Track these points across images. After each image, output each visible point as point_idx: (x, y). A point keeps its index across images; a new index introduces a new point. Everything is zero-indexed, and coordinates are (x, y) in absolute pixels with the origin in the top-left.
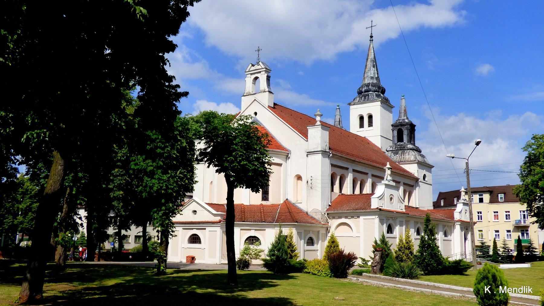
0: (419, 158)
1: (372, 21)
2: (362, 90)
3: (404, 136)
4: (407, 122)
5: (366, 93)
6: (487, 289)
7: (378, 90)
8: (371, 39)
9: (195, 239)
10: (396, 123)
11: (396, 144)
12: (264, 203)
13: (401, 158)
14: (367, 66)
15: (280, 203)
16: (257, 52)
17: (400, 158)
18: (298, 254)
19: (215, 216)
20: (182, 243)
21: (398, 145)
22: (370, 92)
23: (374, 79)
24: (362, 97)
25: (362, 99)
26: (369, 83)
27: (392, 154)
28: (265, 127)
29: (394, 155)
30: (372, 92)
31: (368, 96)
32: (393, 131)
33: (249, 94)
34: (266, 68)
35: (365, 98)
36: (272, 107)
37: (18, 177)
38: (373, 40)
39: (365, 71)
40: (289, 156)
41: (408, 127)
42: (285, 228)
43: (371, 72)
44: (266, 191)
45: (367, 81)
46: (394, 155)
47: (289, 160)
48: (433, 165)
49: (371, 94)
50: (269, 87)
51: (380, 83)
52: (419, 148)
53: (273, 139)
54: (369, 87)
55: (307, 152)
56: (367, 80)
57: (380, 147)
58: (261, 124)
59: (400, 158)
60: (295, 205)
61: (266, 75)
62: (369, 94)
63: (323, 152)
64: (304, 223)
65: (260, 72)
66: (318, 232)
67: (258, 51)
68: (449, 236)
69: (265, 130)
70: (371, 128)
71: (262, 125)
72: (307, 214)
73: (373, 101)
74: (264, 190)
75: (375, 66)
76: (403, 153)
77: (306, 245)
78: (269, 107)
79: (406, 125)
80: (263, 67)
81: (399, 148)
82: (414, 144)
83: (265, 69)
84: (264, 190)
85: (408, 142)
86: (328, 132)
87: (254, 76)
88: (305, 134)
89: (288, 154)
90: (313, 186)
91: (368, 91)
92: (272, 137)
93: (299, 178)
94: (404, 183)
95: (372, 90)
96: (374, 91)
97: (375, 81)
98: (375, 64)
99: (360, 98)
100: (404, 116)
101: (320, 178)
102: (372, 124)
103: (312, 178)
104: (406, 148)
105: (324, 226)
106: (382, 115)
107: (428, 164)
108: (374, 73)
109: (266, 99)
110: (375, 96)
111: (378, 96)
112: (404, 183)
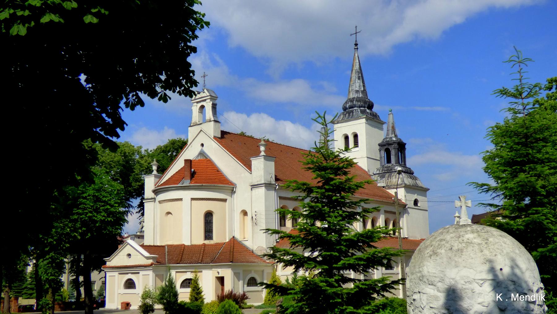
0: (408, 181)
1: (356, 27)
2: (346, 106)
3: (391, 156)
4: (395, 141)
5: (351, 109)
6: (499, 297)
7: (364, 105)
8: (356, 47)
9: (131, 284)
10: (383, 142)
11: (383, 167)
12: (207, 242)
13: (388, 182)
14: (352, 78)
15: (225, 242)
16: (203, 78)
17: (387, 181)
18: (203, 296)
19: (147, 259)
20: (118, 289)
21: (385, 167)
22: (355, 108)
23: (359, 92)
24: (346, 114)
25: (346, 116)
26: (354, 98)
27: (379, 177)
28: (212, 160)
29: (380, 179)
30: (356, 108)
31: (353, 112)
32: (380, 151)
33: (195, 124)
34: (211, 96)
35: (349, 115)
36: (219, 138)
37: (315, 161)
38: (357, 49)
39: (350, 84)
40: (234, 190)
41: (396, 146)
42: (221, 268)
43: (357, 85)
44: (210, 229)
45: (352, 96)
46: (380, 179)
47: (235, 194)
48: (429, 188)
49: (355, 110)
50: (215, 116)
51: (367, 97)
52: (411, 169)
53: (219, 172)
54: (353, 102)
55: (251, 186)
56: (352, 94)
57: (367, 170)
58: (207, 155)
59: (387, 181)
60: (242, 243)
61: (211, 103)
62: (354, 110)
63: (268, 185)
64: (243, 262)
65: (205, 100)
66: (263, 271)
67: (204, 77)
68: (395, 267)
69: (210, 163)
70: (357, 149)
71: (209, 157)
72: (253, 252)
73: (358, 118)
74: (208, 228)
75: (361, 77)
76: (389, 177)
77: (246, 286)
78: (215, 137)
79: (393, 144)
80: (208, 94)
81: (386, 170)
82: (404, 166)
83: (209, 97)
84: (208, 228)
85: (396, 163)
86: (273, 163)
87: (200, 105)
88: (249, 166)
89: (234, 188)
90: (258, 222)
91: (352, 107)
92: (217, 170)
93: (245, 213)
94: (385, 211)
95: (357, 105)
96: (360, 107)
97: (361, 95)
98: (360, 75)
99: (345, 115)
100: (392, 134)
101: (264, 213)
102: (358, 144)
103: (256, 214)
104: (393, 170)
105: (268, 264)
106: (367, 134)
107: (420, 187)
108: (359, 86)
109: (211, 129)
110: (359, 112)
111: (363, 112)
112: (385, 211)
